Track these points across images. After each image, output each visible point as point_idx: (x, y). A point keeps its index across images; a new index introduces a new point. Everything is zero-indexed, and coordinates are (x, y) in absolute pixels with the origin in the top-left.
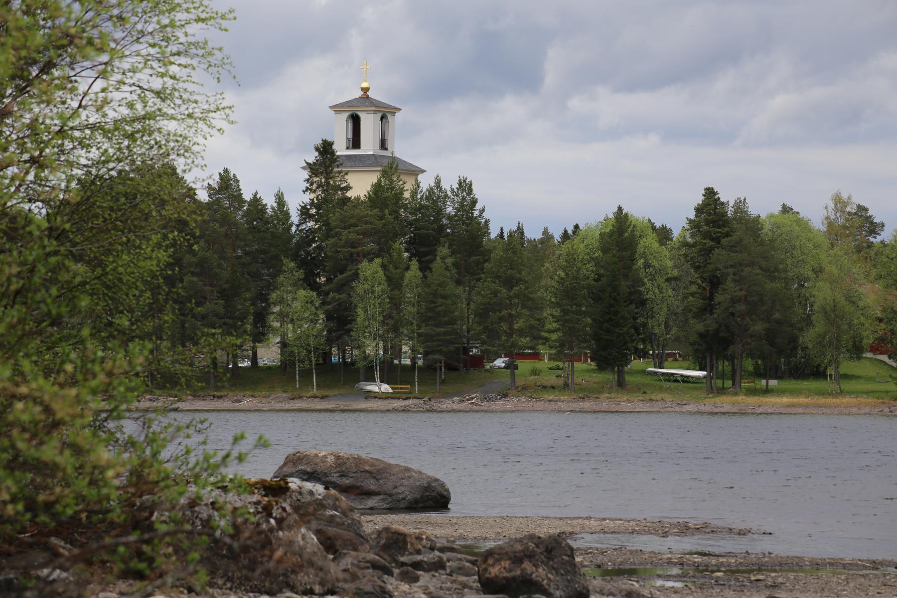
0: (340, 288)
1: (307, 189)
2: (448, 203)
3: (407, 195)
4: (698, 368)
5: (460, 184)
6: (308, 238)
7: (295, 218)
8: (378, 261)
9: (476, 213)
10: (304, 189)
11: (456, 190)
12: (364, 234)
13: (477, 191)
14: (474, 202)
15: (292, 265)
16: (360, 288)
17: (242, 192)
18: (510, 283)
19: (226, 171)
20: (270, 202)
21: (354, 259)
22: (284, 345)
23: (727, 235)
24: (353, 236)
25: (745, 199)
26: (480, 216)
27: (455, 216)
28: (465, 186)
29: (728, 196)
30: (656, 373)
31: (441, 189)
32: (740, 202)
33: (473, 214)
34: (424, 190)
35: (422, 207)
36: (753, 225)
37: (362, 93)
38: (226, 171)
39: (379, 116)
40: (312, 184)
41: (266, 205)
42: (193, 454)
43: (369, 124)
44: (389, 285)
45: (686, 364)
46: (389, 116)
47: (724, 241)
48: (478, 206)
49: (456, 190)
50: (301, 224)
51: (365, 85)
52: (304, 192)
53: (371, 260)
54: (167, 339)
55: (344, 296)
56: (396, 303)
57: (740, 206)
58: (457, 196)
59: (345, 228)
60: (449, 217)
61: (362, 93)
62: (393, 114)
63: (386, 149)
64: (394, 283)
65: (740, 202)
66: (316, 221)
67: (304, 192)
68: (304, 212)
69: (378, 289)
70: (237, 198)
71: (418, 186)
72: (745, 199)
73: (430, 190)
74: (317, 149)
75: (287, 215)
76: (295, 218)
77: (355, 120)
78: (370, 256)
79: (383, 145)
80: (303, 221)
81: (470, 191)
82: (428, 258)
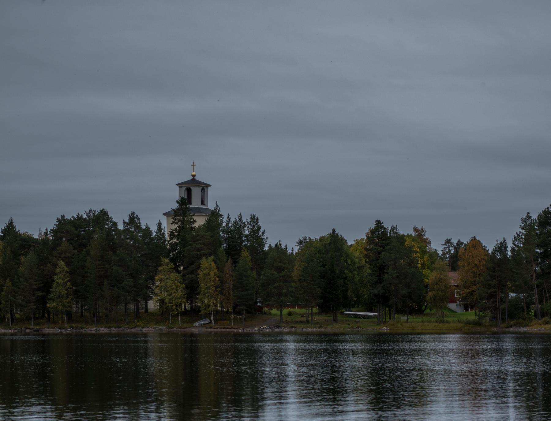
0: (192, 272)
1: (173, 222)
2: (246, 229)
3: (224, 225)
4: (366, 310)
5: (252, 219)
6: (174, 247)
7: (167, 237)
8: (212, 258)
9: (260, 234)
10: (172, 222)
11: (249, 222)
12: (204, 244)
13: (261, 223)
14: (259, 228)
15: (167, 261)
16: (201, 273)
17: (141, 224)
18: (280, 269)
19: (133, 213)
20: (154, 229)
21: (199, 257)
22: (162, 301)
23: (388, 244)
24: (199, 246)
25: (396, 226)
26: (263, 235)
27: (250, 235)
28: (254, 220)
29: (388, 225)
30: (349, 314)
31: (242, 222)
32: (394, 228)
33: (259, 234)
34: (233, 222)
35: (231, 230)
36: (401, 239)
37: (192, 177)
38: (133, 213)
39: (201, 188)
40: (176, 220)
41: (152, 231)
42: (282, 385)
43: (196, 193)
44: (218, 271)
45: (357, 309)
46: (205, 188)
47: (388, 247)
48: (261, 230)
49: (249, 222)
50: (170, 240)
51: (194, 173)
52: (172, 224)
53: (207, 258)
54: (142, 300)
55: (193, 276)
56: (222, 281)
57: (394, 229)
58: (251, 225)
59: (194, 242)
60: (246, 236)
61: (192, 177)
62: (207, 187)
63: (204, 205)
64: (220, 270)
65: (394, 228)
66: (178, 239)
67: (172, 224)
68: (172, 234)
69: (212, 273)
70: (138, 227)
71: (229, 220)
72: (396, 226)
73: (236, 222)
74: (178, 202)
75: (163, 235)
76: (167, 237)
77: (189, 191)
78: (207, 256)
79: (203, 203)
80: (171, 239)
81: (257, 223)
82: (236, 257)
